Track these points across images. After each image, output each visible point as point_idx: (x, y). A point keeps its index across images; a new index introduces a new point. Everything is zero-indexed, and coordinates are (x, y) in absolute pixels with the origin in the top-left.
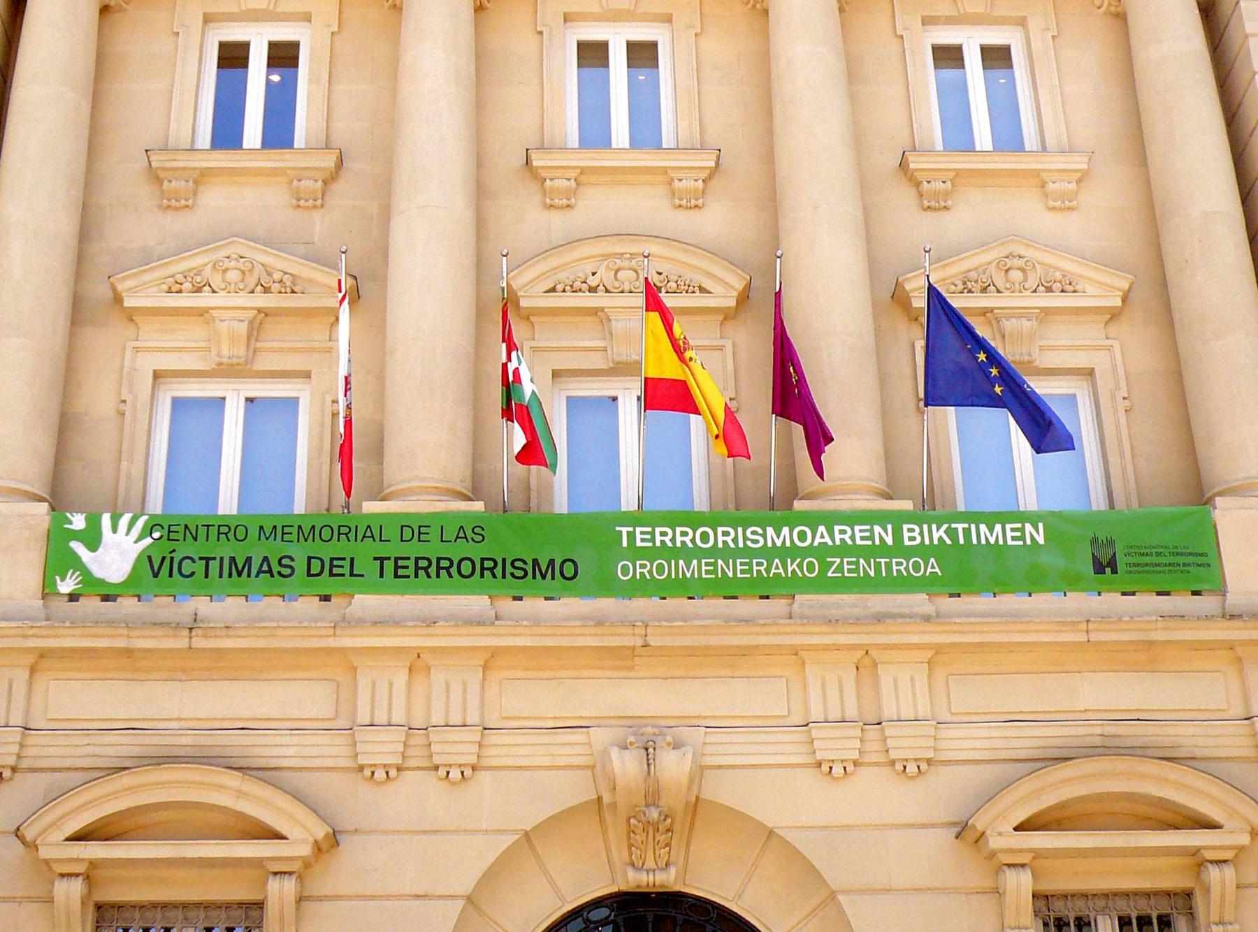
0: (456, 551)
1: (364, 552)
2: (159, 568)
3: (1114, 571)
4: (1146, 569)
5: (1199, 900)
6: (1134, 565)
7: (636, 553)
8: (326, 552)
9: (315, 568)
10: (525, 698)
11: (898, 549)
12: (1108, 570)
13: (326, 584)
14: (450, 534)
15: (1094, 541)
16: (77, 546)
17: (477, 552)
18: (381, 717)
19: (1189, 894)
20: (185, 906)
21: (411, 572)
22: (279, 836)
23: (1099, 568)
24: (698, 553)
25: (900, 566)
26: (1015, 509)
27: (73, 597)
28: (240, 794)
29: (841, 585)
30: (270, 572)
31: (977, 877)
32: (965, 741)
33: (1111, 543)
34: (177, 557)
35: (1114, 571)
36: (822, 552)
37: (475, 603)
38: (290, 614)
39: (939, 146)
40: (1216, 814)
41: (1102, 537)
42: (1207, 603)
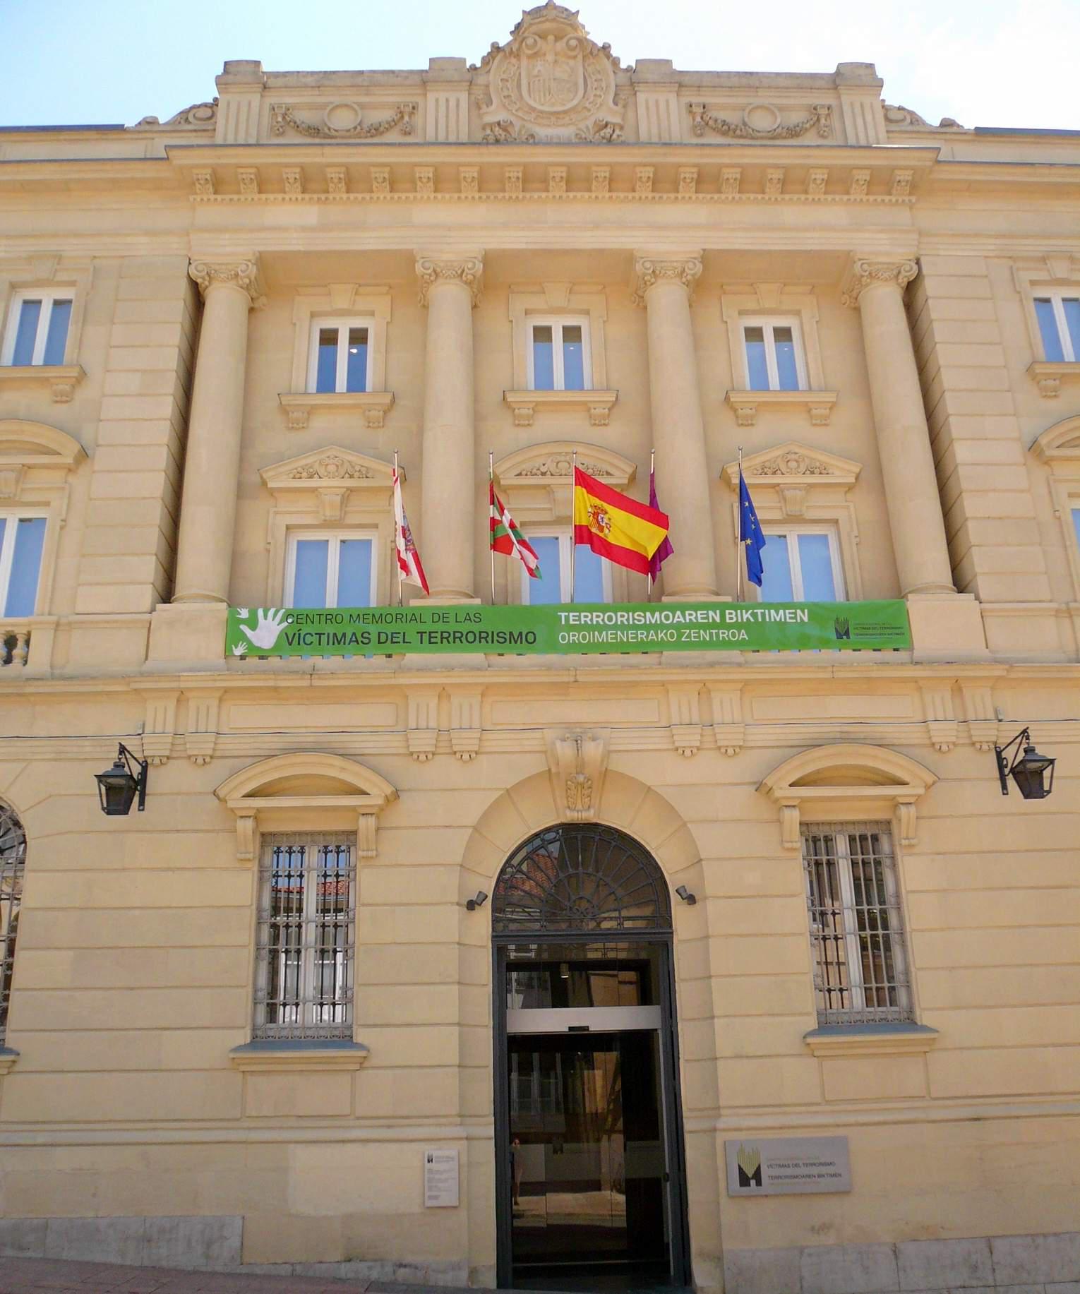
0: (464, 628)
1: (411, 630)
8: (389, 629)
12: (753, 1182)
13: (389, 648)
14: (461, 618)
15: (837, 621)
17: (476, 628)
21: (439, 640)
25: (724, 634)
27: (242, 657)
29: (690, 645)
33: (846, 621)
35: (759, 1183)
36: (678, 627)
37: (475, 657)
38: (366, 665)
40: (906, 778)
41: (842, 619)
42: (903, 656)
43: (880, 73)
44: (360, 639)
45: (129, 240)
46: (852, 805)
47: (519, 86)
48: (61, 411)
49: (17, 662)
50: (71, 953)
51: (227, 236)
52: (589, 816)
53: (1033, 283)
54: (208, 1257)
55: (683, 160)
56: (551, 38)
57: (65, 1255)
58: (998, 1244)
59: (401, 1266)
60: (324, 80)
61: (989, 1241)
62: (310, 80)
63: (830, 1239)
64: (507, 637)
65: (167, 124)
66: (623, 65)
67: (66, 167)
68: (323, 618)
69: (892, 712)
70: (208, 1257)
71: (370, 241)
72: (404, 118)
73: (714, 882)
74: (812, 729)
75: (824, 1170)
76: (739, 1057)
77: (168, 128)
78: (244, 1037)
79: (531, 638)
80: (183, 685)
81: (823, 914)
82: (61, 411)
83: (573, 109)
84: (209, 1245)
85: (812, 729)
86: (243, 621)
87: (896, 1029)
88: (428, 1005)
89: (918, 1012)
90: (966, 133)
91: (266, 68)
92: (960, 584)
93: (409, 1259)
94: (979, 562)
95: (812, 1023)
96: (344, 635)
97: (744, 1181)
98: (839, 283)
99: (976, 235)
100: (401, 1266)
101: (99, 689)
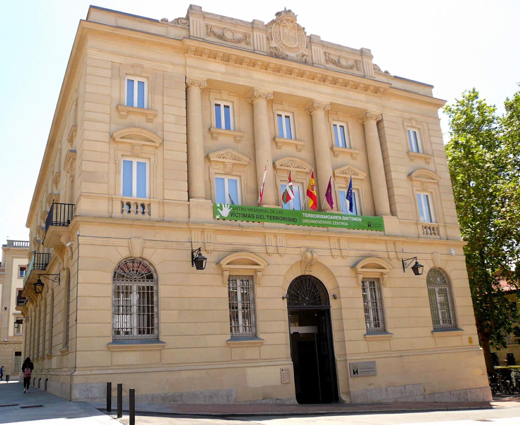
0: (279, 215)
1: (265, 214)
2: (231, 214)
5: (255, 278)
7: (305, 218)
8: (259, 214)
10: (293, 242)
11: (342, 221)
13: (259, 220)
16: (219, 209)
17: (282, 216)
18: (209, 241)
19: (252, 276)
20: (239, 276)
22: (257, 264)
23: (369, 226)
24: (315, 219)
25: (343, 223)
26: (289, 209)
27: (218, 219)
28: (253, 257)
29: (335, 226)
31: (354, 274)
32: (353, 253)
36: (332, 220)
37: (282, 225)
38: (254, 226)
39: (126, 105)
40: (386, 267)
42: (382, 233)
43: (372, 53)
45: (165, 65)
46: (373, 273)
47: (280, 35)
48: (150, 125)
49: (146, 214)
50: (177, 312)
51: (198, 71)
52: (307, 273)
53: (408, 126)
54: (228, 400)
55: (330, 74)
56: (290, 22)
57: (189, 403)
58: (407, 387)
59: (277, 400)
60: (222, 19)
61: (405, 386)
62: (218, 18)
63: (372, 387)
65: (171, 22)
66: (307, 35)
67: (147, 35)
69: (379, 248)
70: (228, 400)
71: (242, 82)
72: (246, 38)
73: (343, 293)
74: (366, 252)
75: (371, 370)
76: (351, 341)
77: (171, 24)
78: (110, 340)
80: (205, 227)
81: (118, 292)
82: (150, 125)
83: (296, 48)
84: (228, 397)
85: (366, 252)
86: (218, 207)
87: (253, 339)
88: (276, 328)
89: (160, 336)
90: (392, 76)
91: (203, 10)
92: (393, 213)
93: (279, 398)
94: (398, 207)
95: (365, 332)
97: (354, 373)
98: (361, 118)
99: (396, 110)
100: (277, 400)
101: (178, 226)
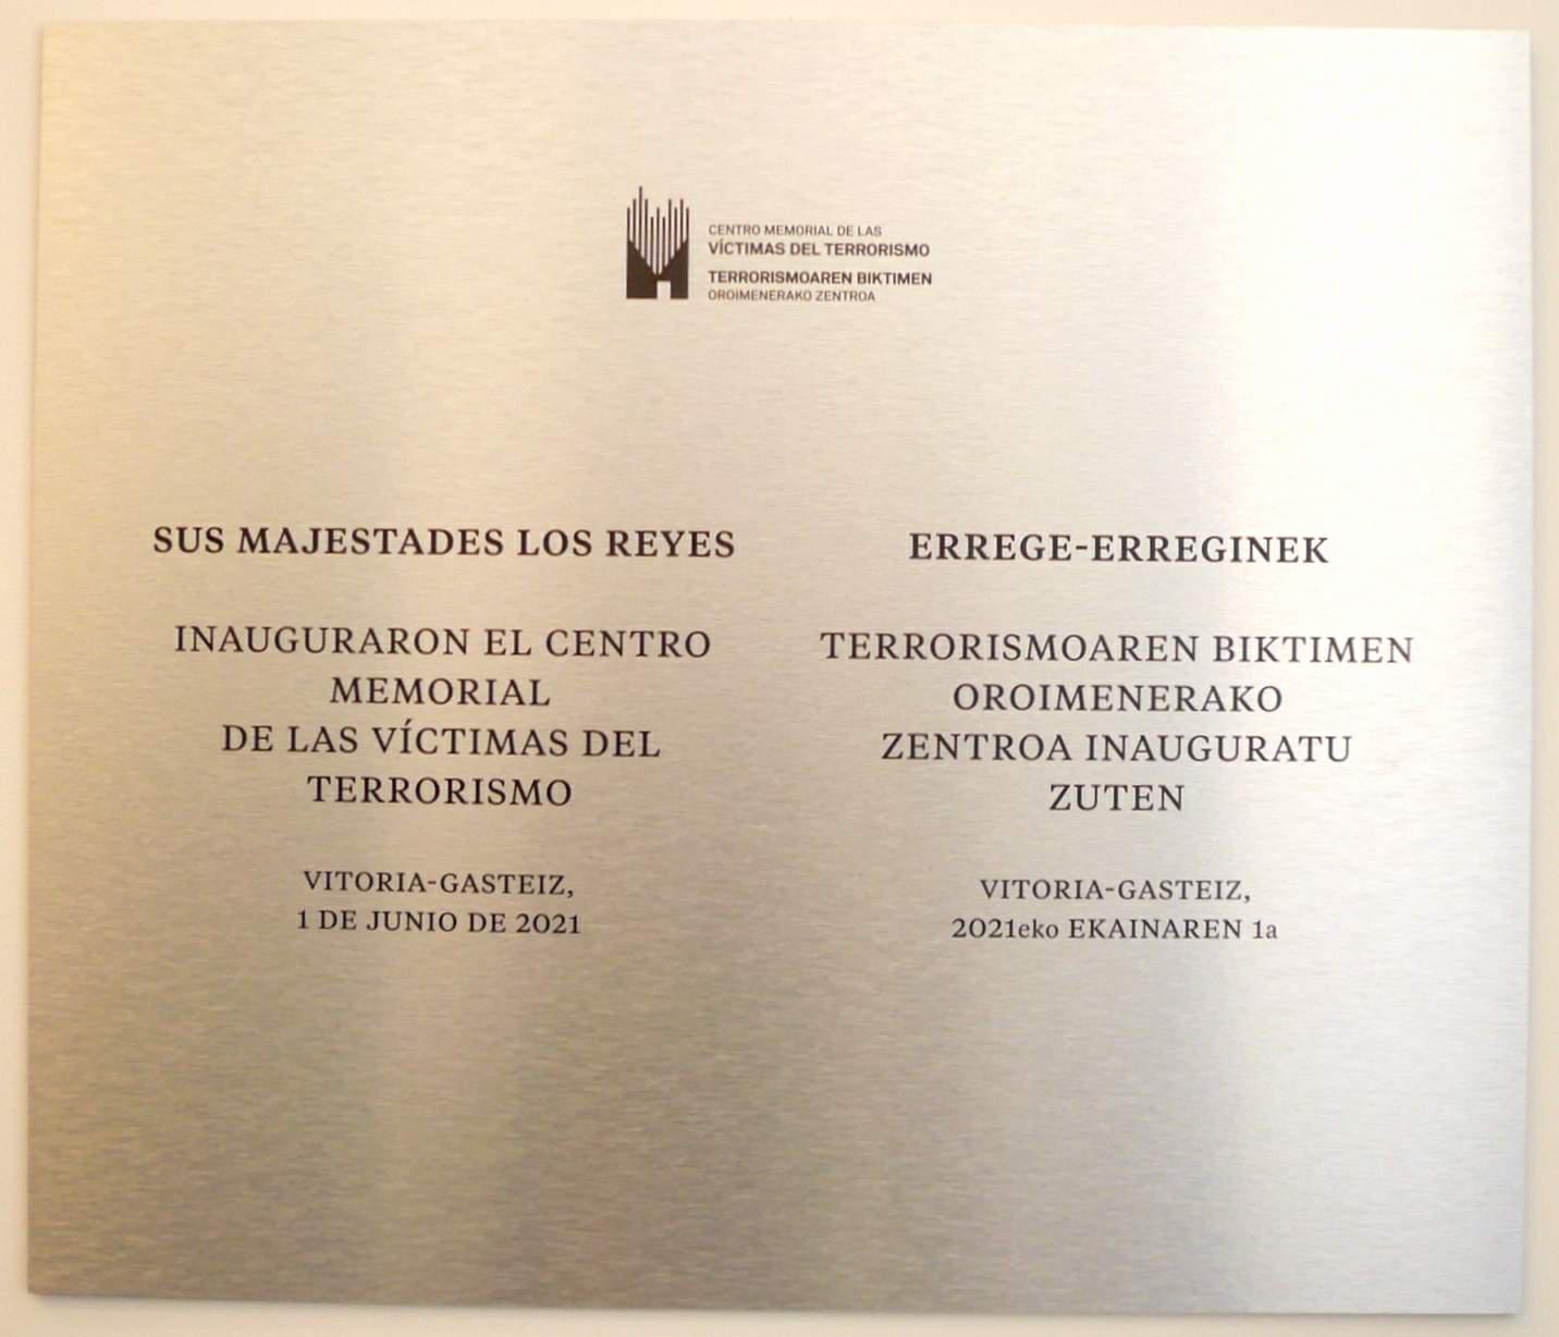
0: (866, 240)
3: (680, 291)
4: (765, 287)
6: (733, 276)
8: (801, 240)
9: (795, 249)
12: (664, 288)
14: (863, 231)
15: (638, 209)
17: (877, 241)
21: (844, 251)
30: (772, 252)
33: (680, 216)
34: (724, 244)
35: (680, 291)
41: (657, 203)
44: (775, 249)
64: (904, 249)
68: (742, 229)
79: (924, 250)
96: (761, 246)
97: (641, 282)
